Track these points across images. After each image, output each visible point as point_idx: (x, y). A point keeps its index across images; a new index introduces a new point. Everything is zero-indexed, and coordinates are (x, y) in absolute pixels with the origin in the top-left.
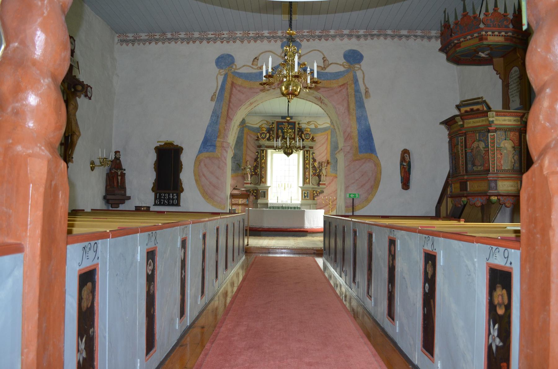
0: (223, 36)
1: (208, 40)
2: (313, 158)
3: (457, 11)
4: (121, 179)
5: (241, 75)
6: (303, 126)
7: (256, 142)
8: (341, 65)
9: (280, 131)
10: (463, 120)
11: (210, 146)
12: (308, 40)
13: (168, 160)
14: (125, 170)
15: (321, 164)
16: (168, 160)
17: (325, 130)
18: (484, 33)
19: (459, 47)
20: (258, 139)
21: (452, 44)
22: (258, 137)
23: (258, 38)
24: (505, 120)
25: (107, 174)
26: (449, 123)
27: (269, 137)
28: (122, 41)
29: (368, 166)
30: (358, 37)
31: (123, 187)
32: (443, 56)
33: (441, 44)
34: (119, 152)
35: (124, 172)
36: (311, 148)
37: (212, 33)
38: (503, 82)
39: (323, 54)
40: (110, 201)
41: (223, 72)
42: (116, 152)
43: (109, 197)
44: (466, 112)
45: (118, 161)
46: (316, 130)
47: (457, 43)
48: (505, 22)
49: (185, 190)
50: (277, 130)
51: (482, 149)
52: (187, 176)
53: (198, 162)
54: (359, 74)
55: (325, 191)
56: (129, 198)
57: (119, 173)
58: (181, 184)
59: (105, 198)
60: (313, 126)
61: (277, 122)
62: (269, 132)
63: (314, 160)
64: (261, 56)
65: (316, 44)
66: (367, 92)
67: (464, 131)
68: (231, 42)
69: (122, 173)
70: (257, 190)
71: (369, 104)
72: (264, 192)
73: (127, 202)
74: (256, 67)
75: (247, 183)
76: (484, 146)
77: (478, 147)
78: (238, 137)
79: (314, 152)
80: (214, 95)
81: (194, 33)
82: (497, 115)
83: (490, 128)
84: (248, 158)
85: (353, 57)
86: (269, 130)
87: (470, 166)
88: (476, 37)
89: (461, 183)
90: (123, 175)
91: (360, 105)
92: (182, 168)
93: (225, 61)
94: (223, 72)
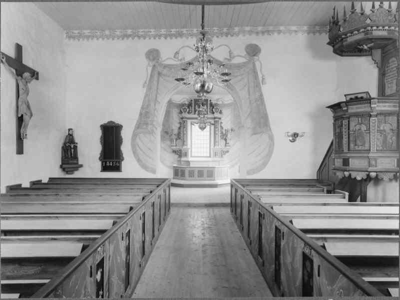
0: (151, 33)
1: (139, 37)
2: (221, 126)
3: (346, 10)
4: (74, 151)
5: (165, 66)
6: (214, 102)
7: (180, 115)
8: (243, 57)
9: (197, 106)
10: (347, 106)
11: (144, 124)
12: (218, 37)
13: (111, 136)
14: (77, 143)
15: (227, 131)
16: (111, 136)
17: (229, 105)
18: (369, 28)
19: (346, 41)
20: (181, 112)
21: (340, 39)
22: (181, 111)
23: (180, 35)
24: (385, 106)
25: (63, 147)
26: (336, 107)
27: (189, 110)
28: (70, 37)
29: (265, 137)
30: (257, 33)
31: (75, 157)
32: (331, 48)
33: (330, 39)
34: (72, 129)
35: (76, 145)
36: (220, 119)
37: (142, 30)
38: (380, 70)
39: (229, 48)
40: (66, 170)
41: (152, 64)
42: (69, 130)
43: (64, 166)
44: (351, 99)
45: (71, 137)
46: (225, 105)
47: (344, 38)
48: (389, 17)
49: (125, 159)
50: (195, 106)
51: (364, 132)
52: (126, 148)
53: (135, 136)
54: (257, 64)
55: (230, 151)
56: (81, 166)
57: (72, 146)
58: (122, 154)
59: (61, 166)
60: (221, 103)
61: (195, 100)
62: (189, 107)
63: (222, 128)
64: (182, 50)
65: (223, 40)
66: (263, 79)
67: (348, 116)
68: (157, 38)
69: (74, 146)
70: (180, 150)
71: (265, 89)
72: (186, 153)
73: (80, 169)
74: (177, 60)
75: (173, 146)
76: (365, 129)
77: (360, 129)
78: (166, 111)
79: (222, 122)
80: (145, 83)
81: (127, 30)
82: (379, 102)
83: (371, 114)
84: (174, 128)
85: (253, 51)
86: (190, 105)
87: (352, 145)
88: (362, 32)
89: (343, 159)
90: (75, 148)
91: (258, 86)
92: (122, 142)
93: (153, 55)
94: (152, 64)
